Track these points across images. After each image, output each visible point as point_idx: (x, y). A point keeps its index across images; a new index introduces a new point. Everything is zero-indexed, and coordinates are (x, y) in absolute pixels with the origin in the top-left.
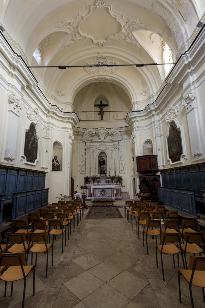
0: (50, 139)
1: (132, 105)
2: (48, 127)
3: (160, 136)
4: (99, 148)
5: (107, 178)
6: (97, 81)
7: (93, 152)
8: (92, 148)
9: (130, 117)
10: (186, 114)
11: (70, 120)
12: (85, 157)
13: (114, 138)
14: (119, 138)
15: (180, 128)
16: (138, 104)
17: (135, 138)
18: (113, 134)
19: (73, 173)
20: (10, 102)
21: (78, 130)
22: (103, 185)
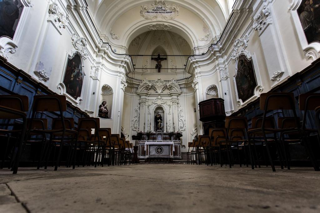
0: (99, 81)
1: (193, 51)
2: (97, 67)
3: (225, 79)
4: (156, 103)
5: (165, 134)
6: (155, 28)
7: (148, 107)
8: (148, 102)
9: (191, 62)
10: (259, 36)
11: (123, 64)
12: (139, 111)
13: (172, 91)
14: (178, 91)
15: (251, 58)
16: (200, 49)
17: (196, 85)
18: (172, 87)
19: (124, 129)
20: (51, 12)
21: (132, 81)
22: (159, 141)
